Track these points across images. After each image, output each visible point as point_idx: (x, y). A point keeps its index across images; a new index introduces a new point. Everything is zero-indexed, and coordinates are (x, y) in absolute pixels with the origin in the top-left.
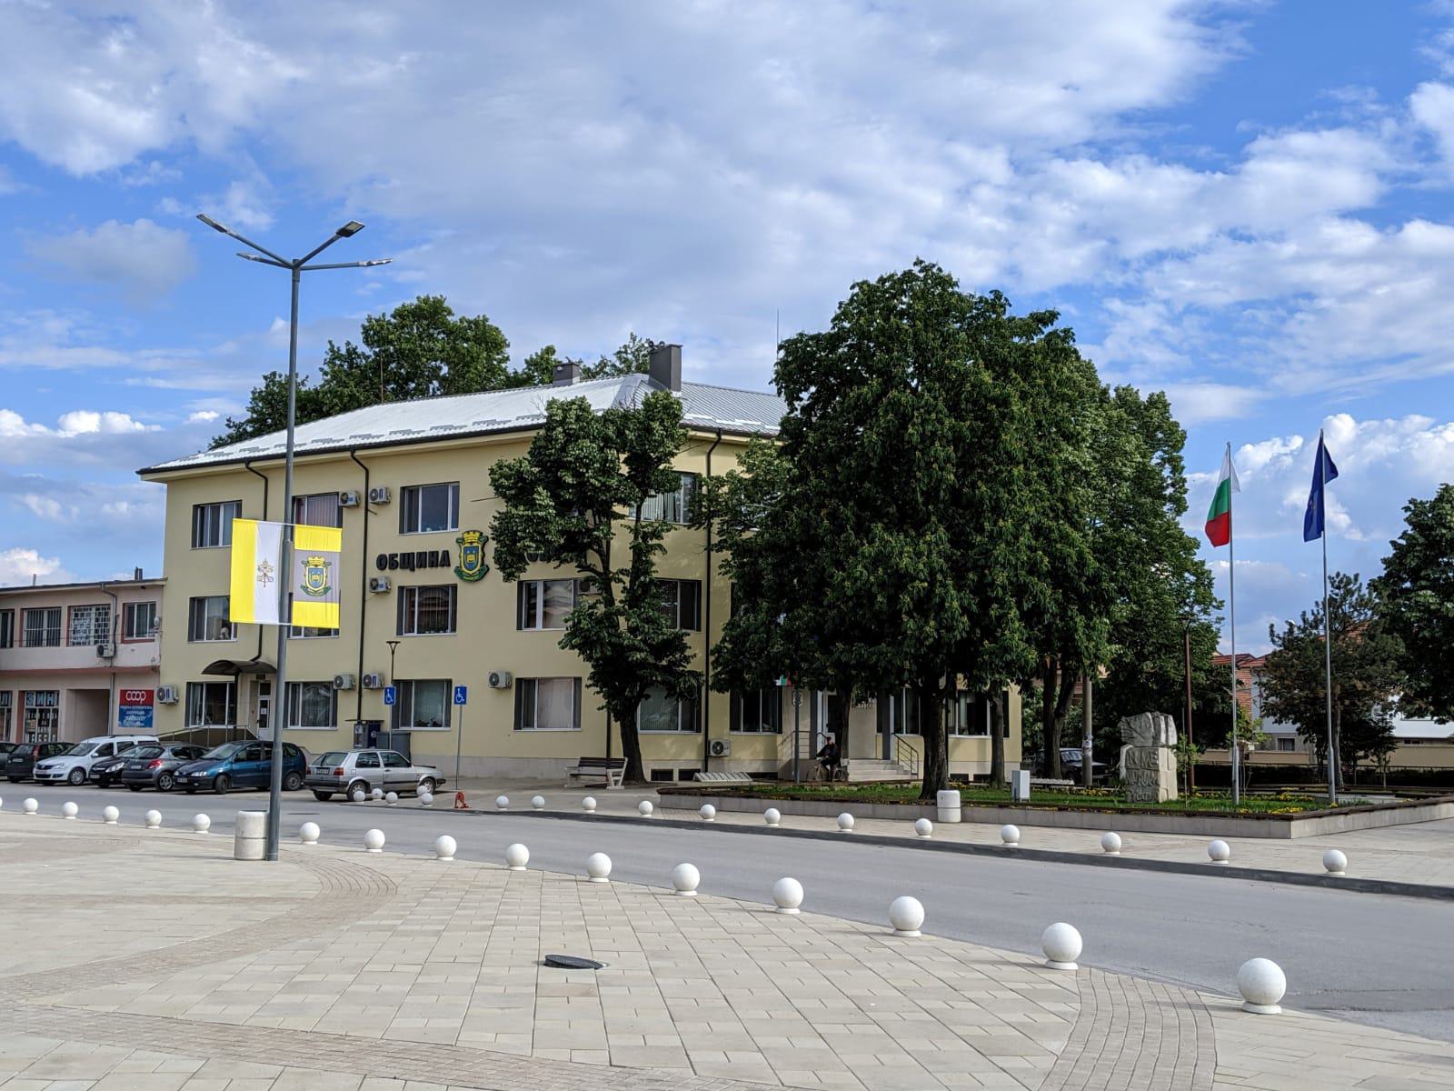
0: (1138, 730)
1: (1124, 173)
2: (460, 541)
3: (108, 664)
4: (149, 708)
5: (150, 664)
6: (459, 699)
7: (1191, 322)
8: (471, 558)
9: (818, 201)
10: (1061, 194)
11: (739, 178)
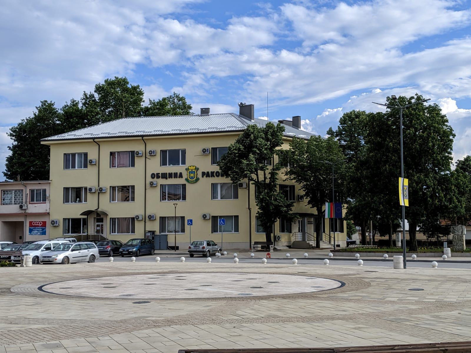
0: (457, 230)
1: (186, 26)
2: (187, 169)
3: (23, 212)
4: (44, 228)
5: (45, 212)
6: (190, 223)
7: (212, 82)
8: (192, 175)
9: (71, 25)
10: (164, 31)
11: (37, 13)
